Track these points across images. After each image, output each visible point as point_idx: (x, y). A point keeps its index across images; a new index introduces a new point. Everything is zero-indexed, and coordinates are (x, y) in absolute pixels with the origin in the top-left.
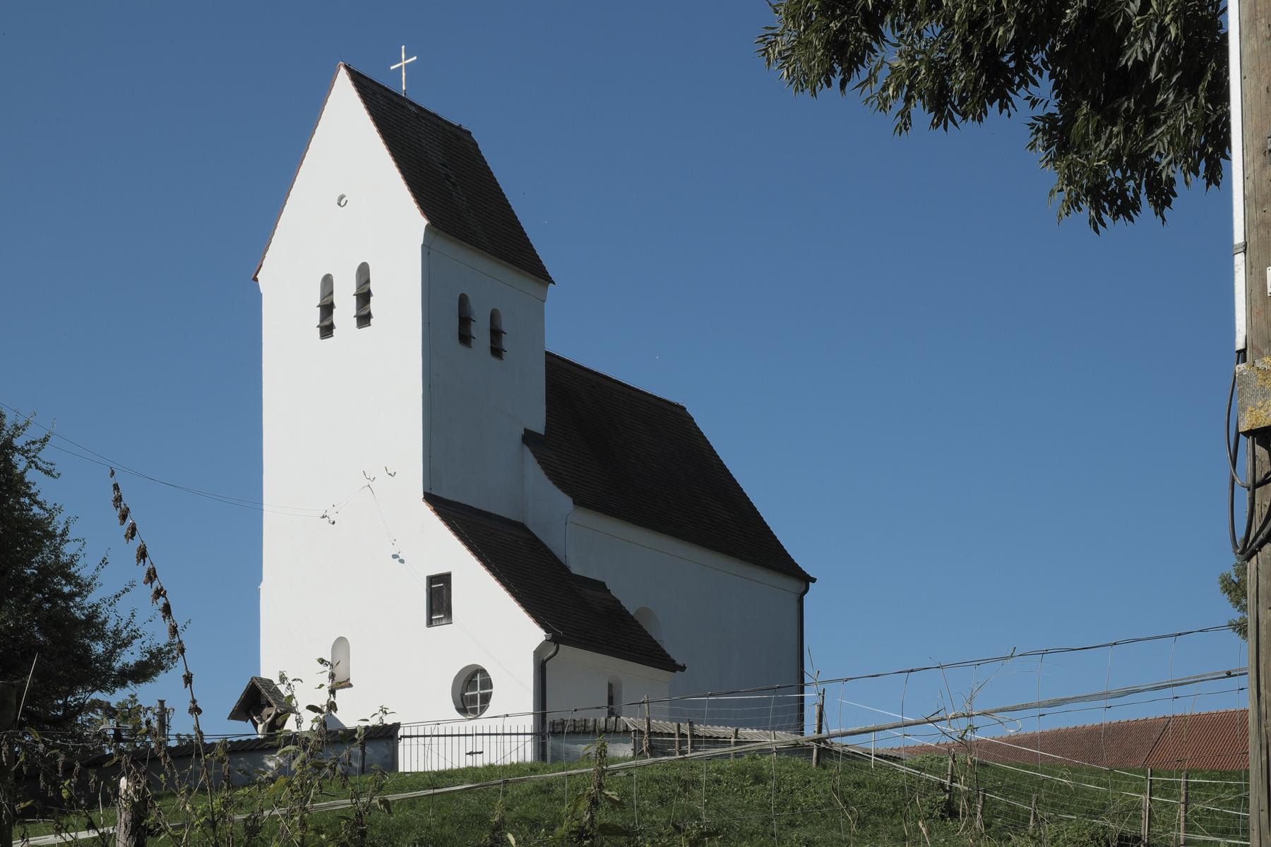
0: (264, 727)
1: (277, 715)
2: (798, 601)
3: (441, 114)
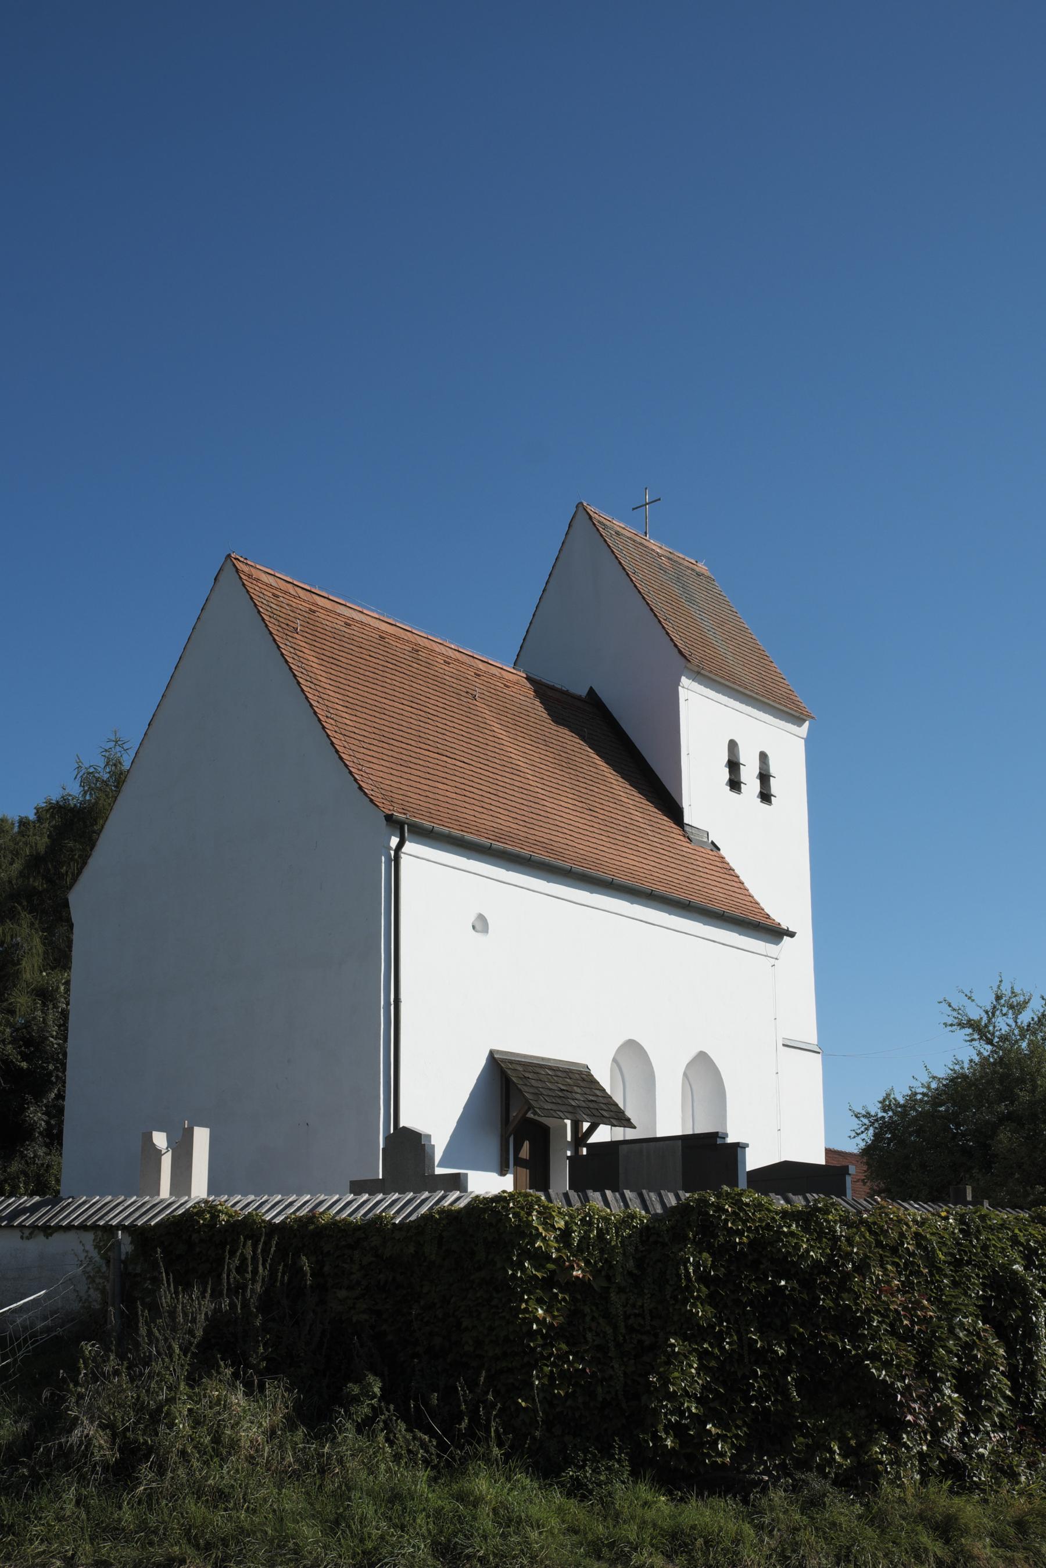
2: (65, 1232)
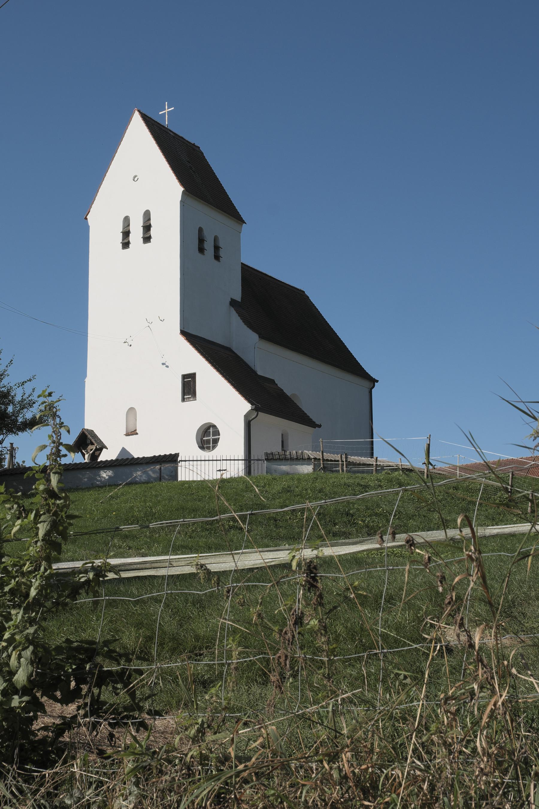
0: (89, 456)
1: (96, 450)
3: (184, 137)
